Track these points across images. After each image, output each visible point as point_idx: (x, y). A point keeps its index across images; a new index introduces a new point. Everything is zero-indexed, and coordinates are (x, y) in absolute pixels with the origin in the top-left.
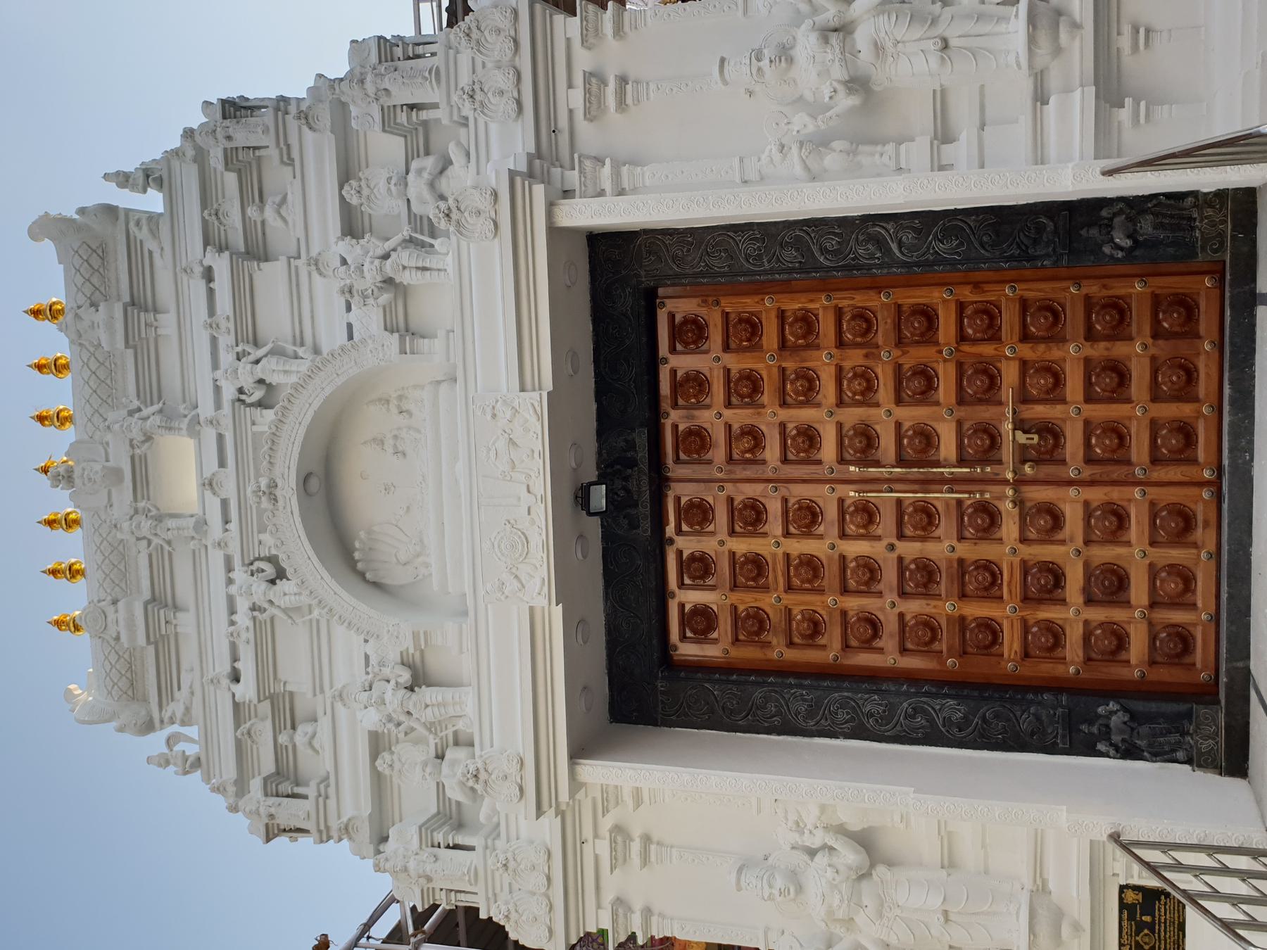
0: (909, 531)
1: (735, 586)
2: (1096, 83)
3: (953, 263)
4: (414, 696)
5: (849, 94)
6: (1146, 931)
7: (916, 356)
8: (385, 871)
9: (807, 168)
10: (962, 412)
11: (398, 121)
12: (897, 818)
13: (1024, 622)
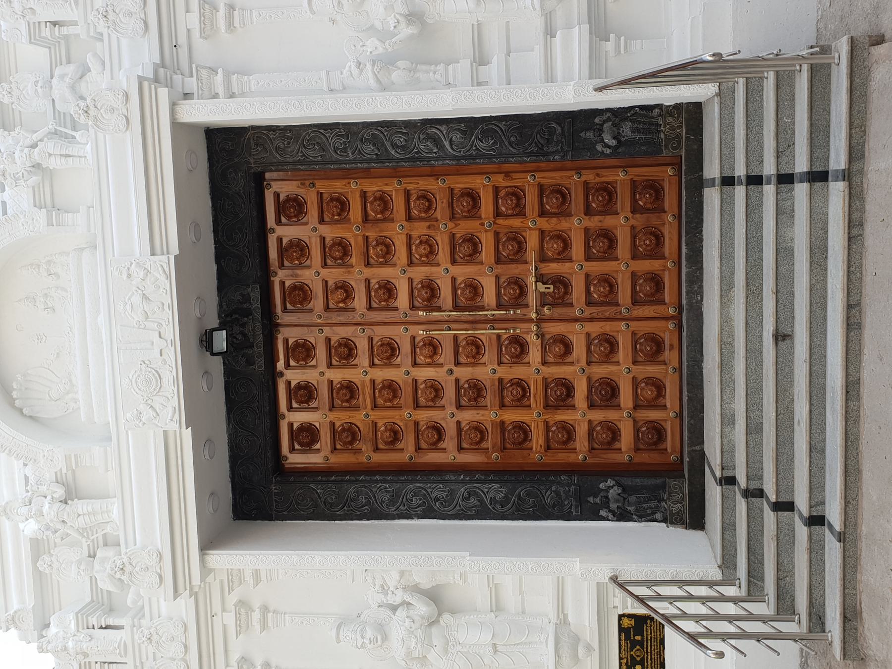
0: (463, 359)
1: (332, 407)
2: (589, 23)
3: (490, 157)
4: (68, 508)
5: (408, 25)
6: (638, 647)
7: (465, 227)
8: (48, 651)
9: (378, 81)
10: (499, 269)
11: (43, 35)
12: (457, 577)
13: (546, 423)
